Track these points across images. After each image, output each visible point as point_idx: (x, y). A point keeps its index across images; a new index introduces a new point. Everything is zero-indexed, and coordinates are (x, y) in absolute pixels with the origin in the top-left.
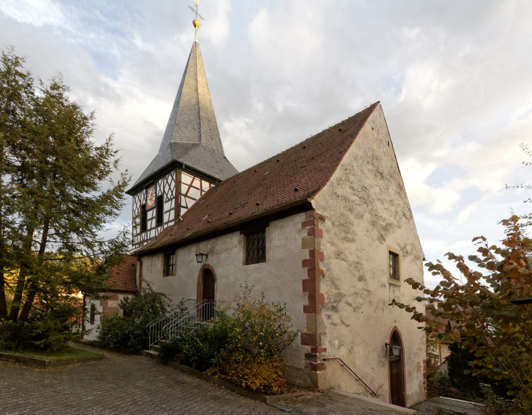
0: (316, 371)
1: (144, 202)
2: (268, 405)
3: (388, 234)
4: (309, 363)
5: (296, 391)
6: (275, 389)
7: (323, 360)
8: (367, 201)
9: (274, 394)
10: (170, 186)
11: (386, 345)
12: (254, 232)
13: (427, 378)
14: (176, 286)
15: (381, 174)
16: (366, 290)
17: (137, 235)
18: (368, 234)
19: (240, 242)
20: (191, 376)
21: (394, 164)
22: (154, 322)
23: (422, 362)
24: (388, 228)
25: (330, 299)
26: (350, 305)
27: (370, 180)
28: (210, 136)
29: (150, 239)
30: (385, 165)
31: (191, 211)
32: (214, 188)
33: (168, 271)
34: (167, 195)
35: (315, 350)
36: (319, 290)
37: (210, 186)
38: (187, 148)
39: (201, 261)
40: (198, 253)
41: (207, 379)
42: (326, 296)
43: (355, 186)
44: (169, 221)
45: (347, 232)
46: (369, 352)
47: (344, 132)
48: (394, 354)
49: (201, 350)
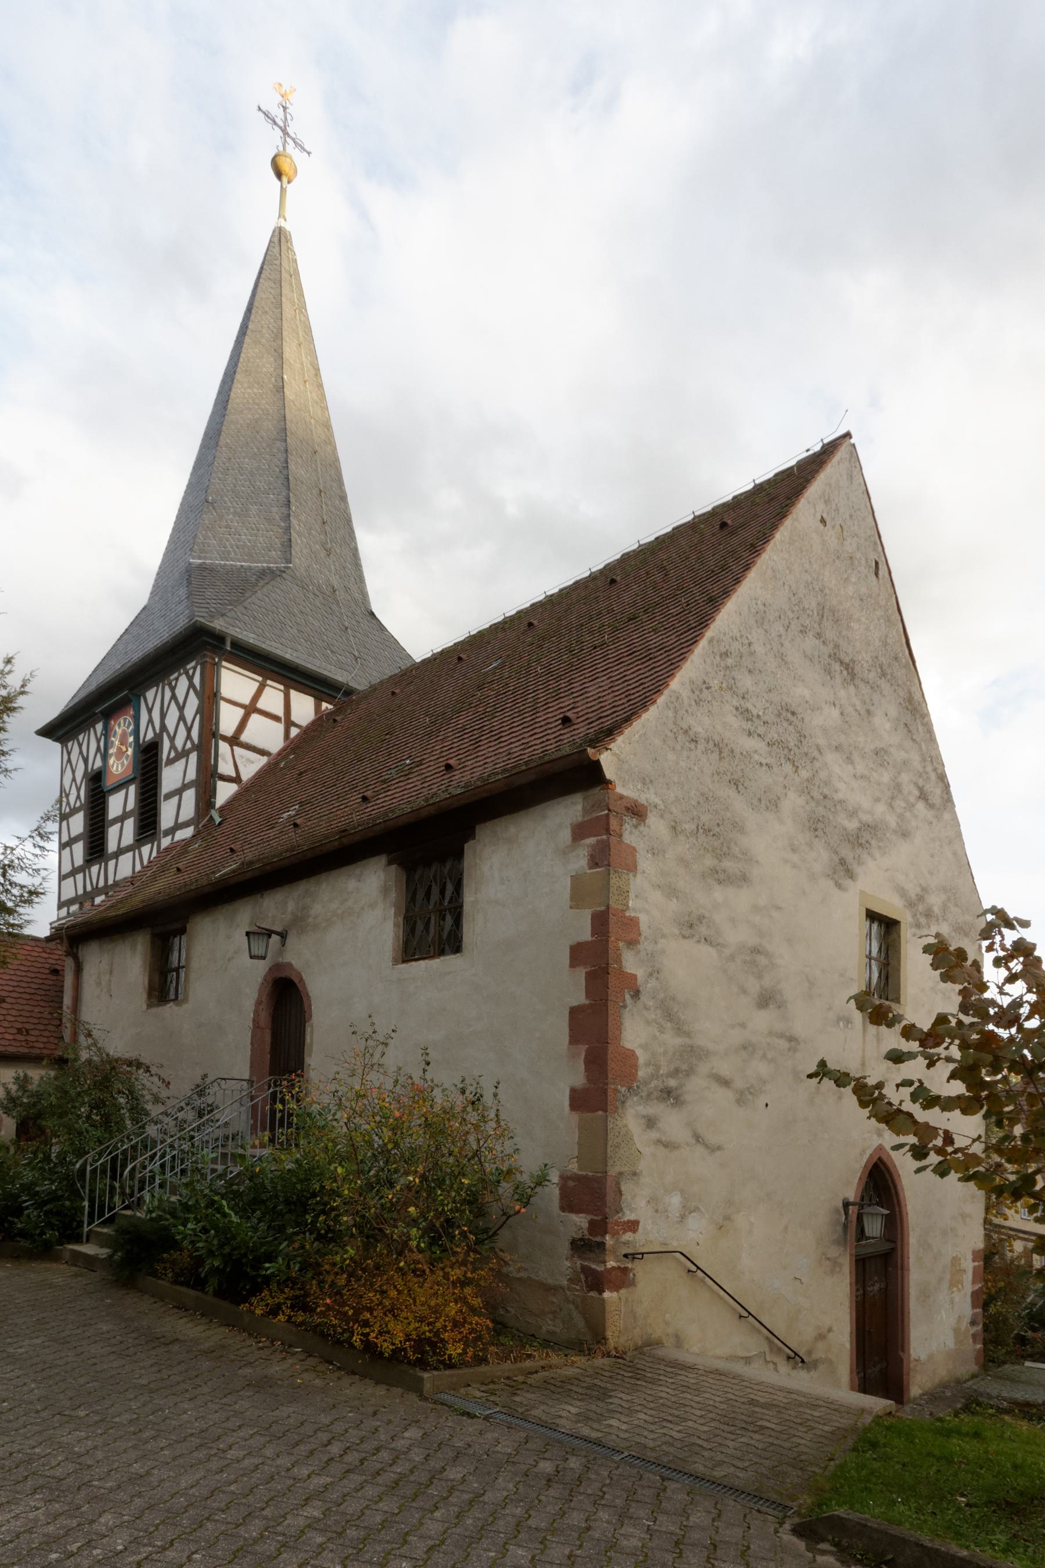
0: (601, 1292)
1: (98, 763)
2: (426, 1399)
3: (864, 855)
4: (583, 1267)
5: (529, 1356)
6: (454, 1350)
7: (626, 1256)
8: (794, 749)
9: (451, 1366)
10: (181, 708)
11: (846, 1205)
12: (427, 856)
13: (985, 1306)
14: (181, 1039)
15: (849, 667)
16: (781, 1036)
17: (74, 872)
18: (795, 858)
19: (385, 891)
20: (204, 1320)
21: (895, 633)
22: (100, 1155)
23: (970, 1257)
24: (864, 838)
25: (658, 1067)
26: (725, 1083)
27: (807, 687)
28: (323, 545)
29: (116, 883)
30: (863, 637)
31: (251, 791)
32: (330, 714)
33: (163, 986)
34: (172, 739)
35: (599, 1227)
36: (618, 1038)
37: (317, 707)
38: (242, 584)
39: (261, 952)
40: (254, 929)
41: (251, 1329)
42: (642, 1057)
43: (756, 706)
44: (178, 826)
45: (721, 855)
46: (786, 1228)
47: (733, 533)
48: (868, 1232)
49: (234, 1237)
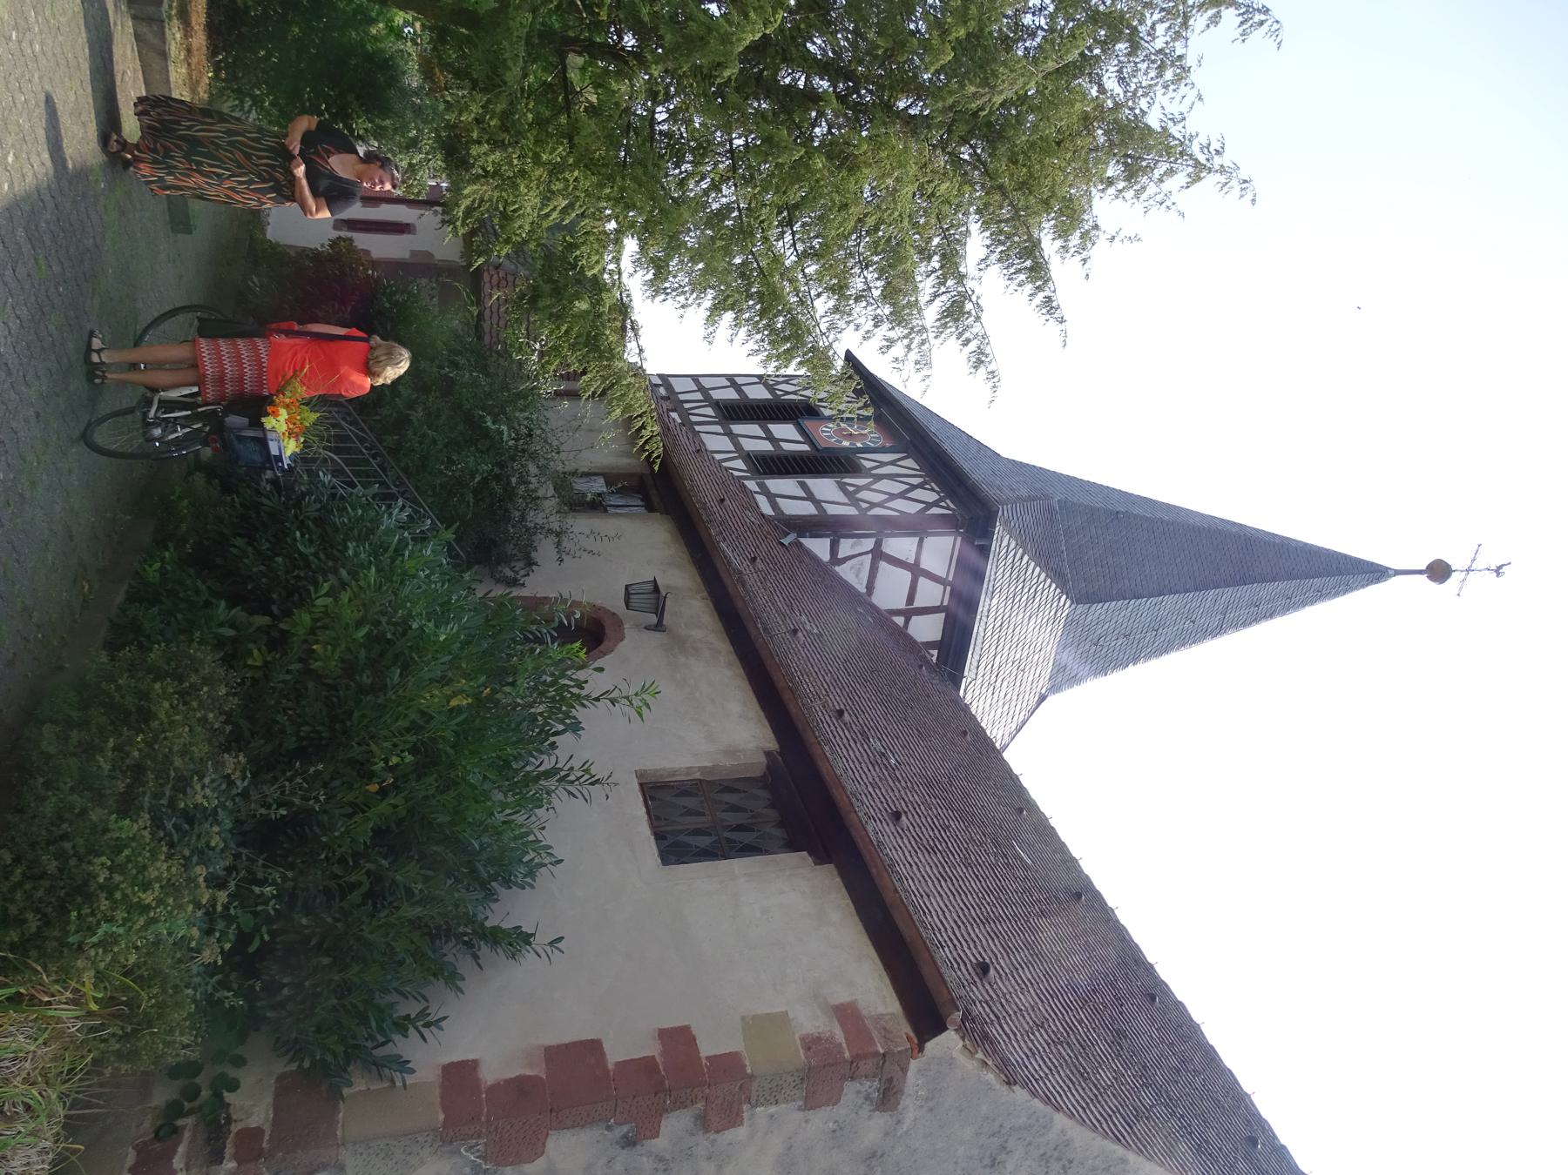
19: (731, 752)
44: (772, 498)
47: (1248, 1157)
